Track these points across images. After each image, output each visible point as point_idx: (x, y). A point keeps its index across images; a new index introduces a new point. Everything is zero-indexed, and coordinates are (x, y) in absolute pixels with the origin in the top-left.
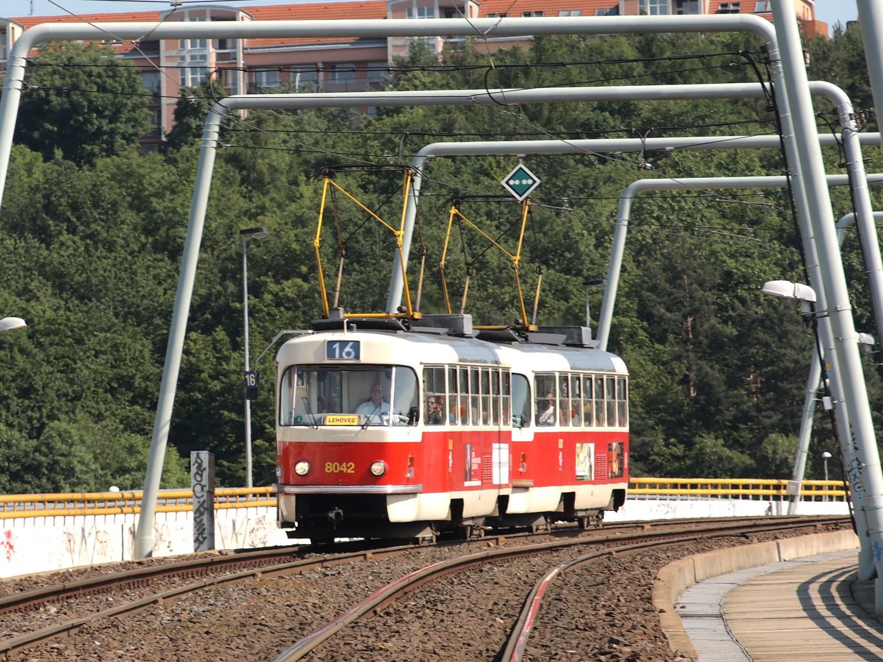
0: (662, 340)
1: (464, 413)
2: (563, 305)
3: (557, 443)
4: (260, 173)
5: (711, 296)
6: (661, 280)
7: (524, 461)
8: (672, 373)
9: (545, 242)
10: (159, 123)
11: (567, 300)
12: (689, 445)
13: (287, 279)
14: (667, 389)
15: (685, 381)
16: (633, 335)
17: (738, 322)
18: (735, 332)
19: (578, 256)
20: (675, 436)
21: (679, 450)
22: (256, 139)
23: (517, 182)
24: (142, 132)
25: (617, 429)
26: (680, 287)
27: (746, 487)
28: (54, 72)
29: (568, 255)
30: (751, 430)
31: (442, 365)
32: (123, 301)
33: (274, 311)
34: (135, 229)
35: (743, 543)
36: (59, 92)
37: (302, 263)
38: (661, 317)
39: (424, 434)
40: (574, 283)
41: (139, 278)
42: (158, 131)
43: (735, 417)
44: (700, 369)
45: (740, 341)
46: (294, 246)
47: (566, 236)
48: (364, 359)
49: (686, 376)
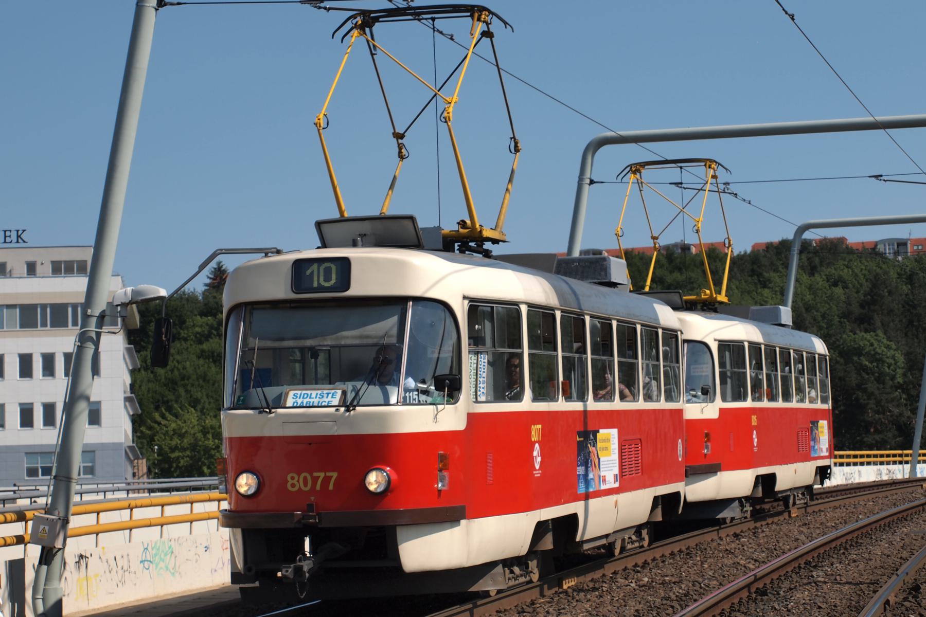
1: (800, 390)
3: (750, 419)
7: (708, 440)
25: (819, 405)
27: (888, 456)
31: (742, 342)
39: (722, 411)
48: (356, 289)
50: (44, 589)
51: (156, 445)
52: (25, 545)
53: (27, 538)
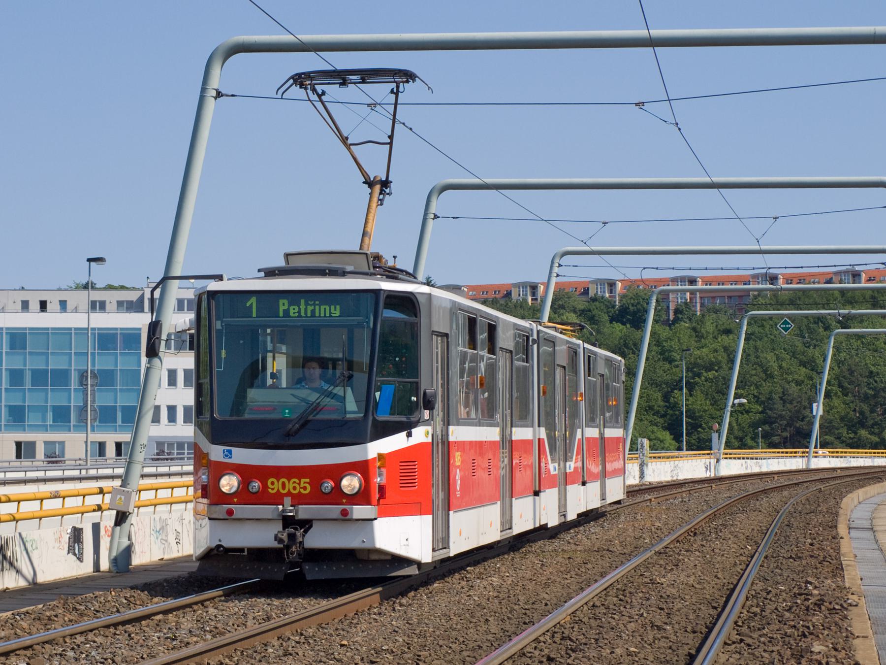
0: (846, 395)
2: (811, 382)
4: (703, 334)
5: (865, 380)
6: (847, 374)
8: (850, 408)
9: (805, 359)
10: (669, 317)
11: (812, 380)
12: (856, 433)
13: (710, 371)
14: (848, 413)
15: (855, 410)
16: (836, 394)
17: (874, 389)
18: (873, 393)
19: (816, 364)
20: (851, 430)
21: (852, 436)
22: (702, 322)
23: (787, 326)
24: (662, 319)
26: (853, 376)
28: (631, 298)
29: (813, 364)
30: (878, 428)
32: (651, 379)
33: (705, 383)
34: (657, 353)
35: (879, 482)
36: (633, 305)
37: (716, 366)
38: (846, 387)
40: (814, 374)
41: (657, 370)
42: (669, 320)
43: (873, 424)
44: (860, 406)
45: (875, 396)
46: (713, 359)
47: (813, 357)
49: (855, 409)
50: (119, 542)
51: (395, 360)
52: (102, 512)
53: (104, 507)
